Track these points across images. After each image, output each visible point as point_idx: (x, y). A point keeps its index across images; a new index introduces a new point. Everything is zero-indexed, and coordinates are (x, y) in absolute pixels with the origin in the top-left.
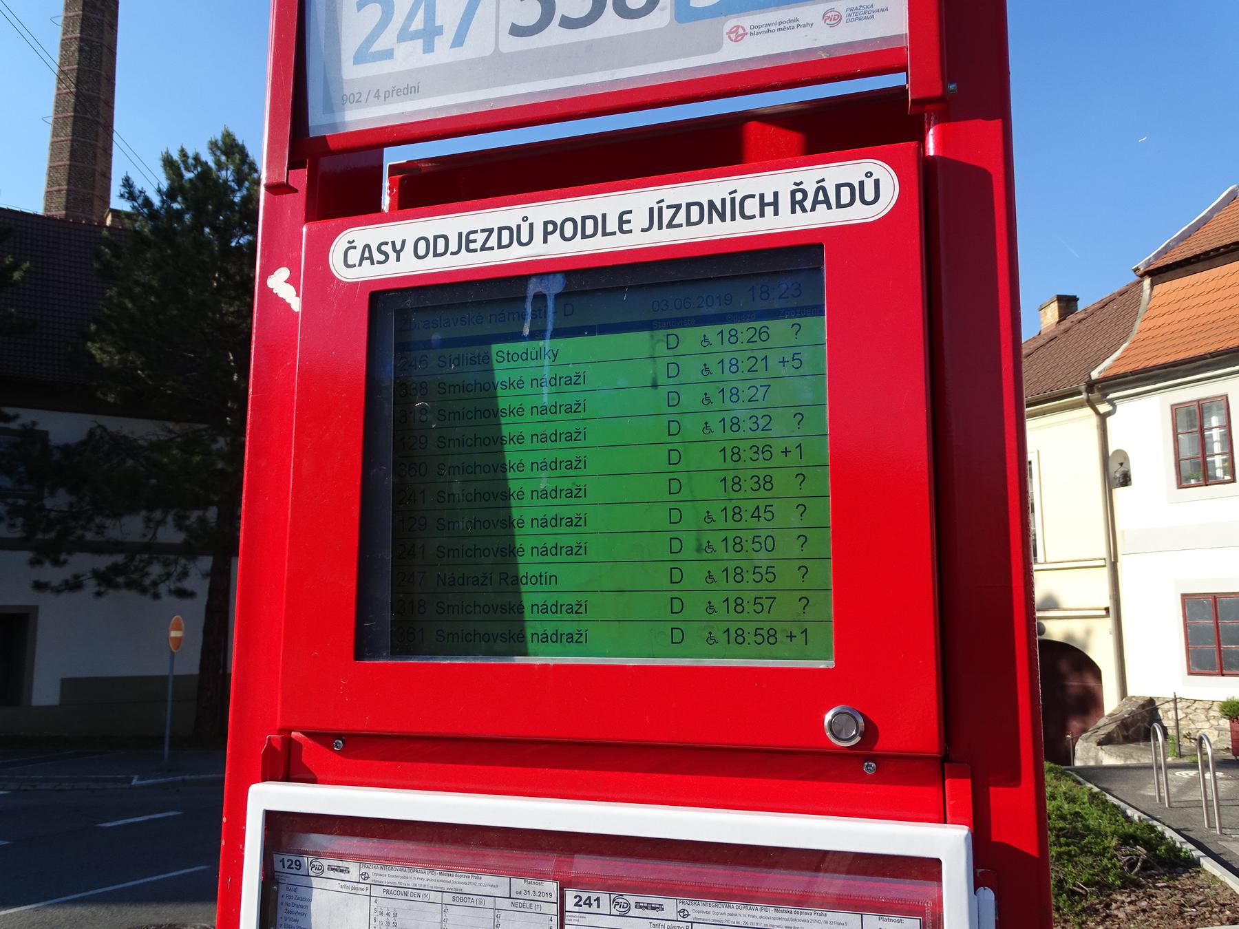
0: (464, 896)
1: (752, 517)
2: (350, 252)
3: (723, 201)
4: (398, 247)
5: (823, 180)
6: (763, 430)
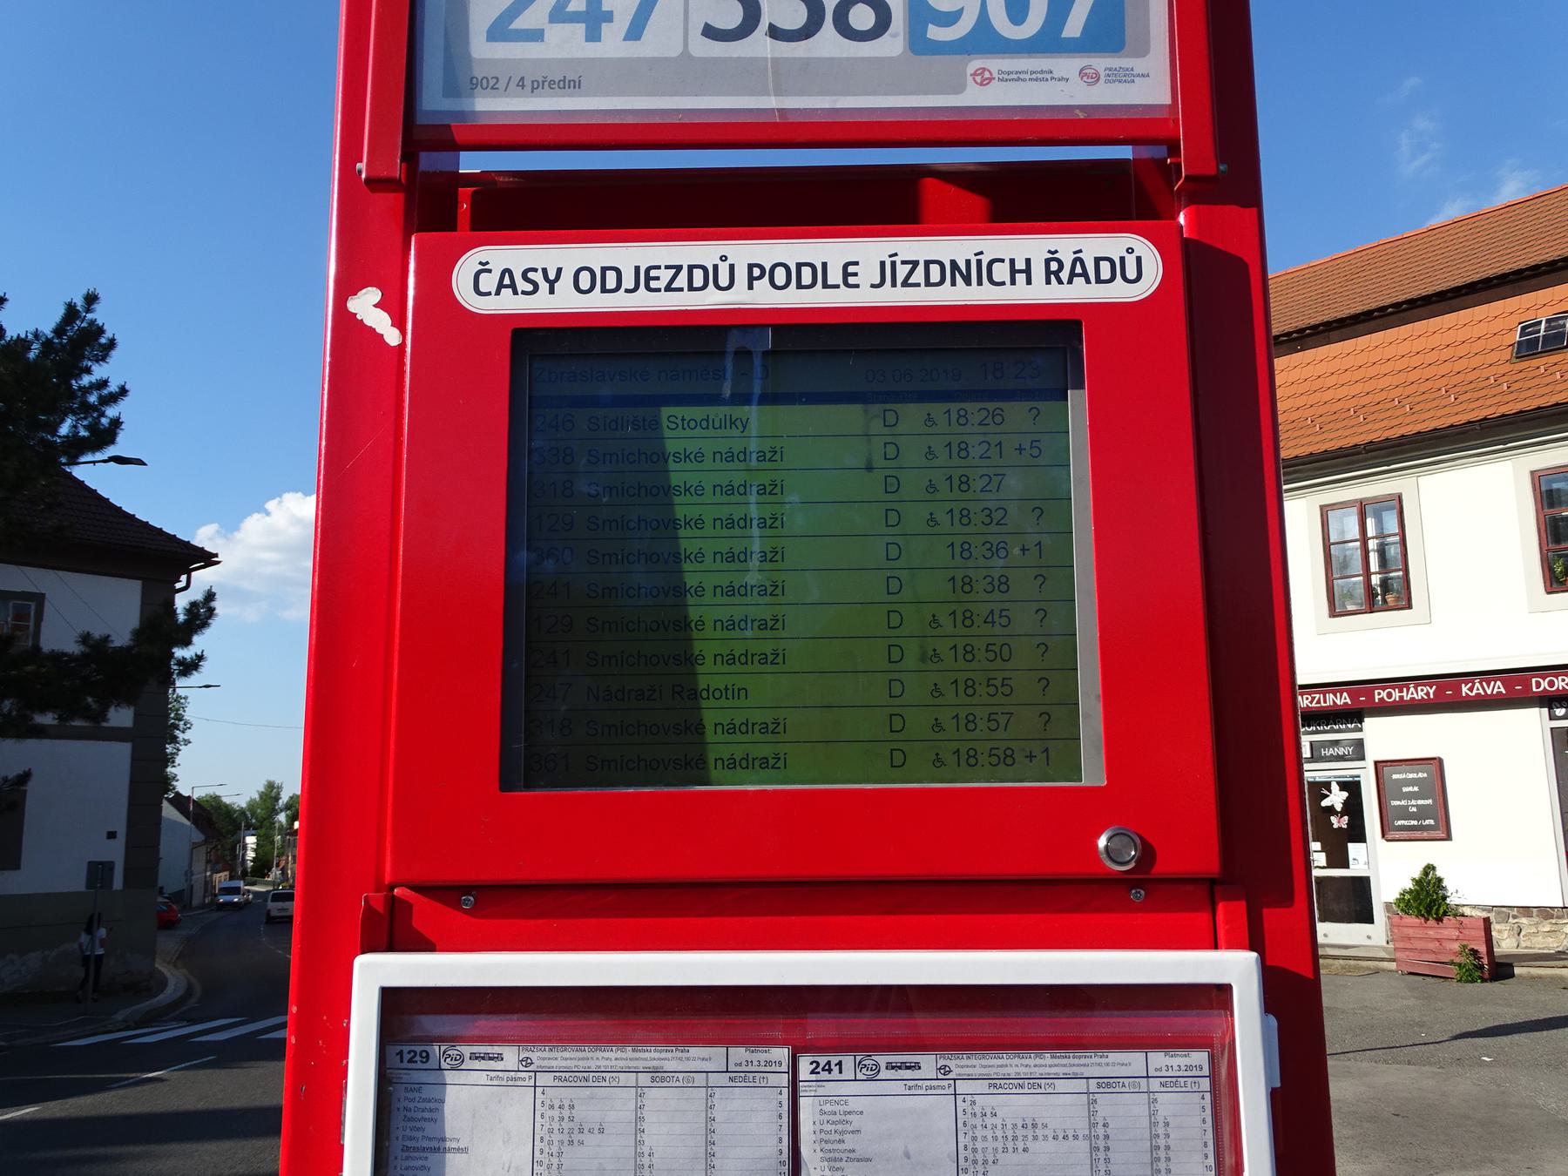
0: (1112, 1081)
1: (985, 622)
2: (483, 276)
3: (968, 262)
4: (552, 276)
5: (1080, 251)
6: (997, 524)
